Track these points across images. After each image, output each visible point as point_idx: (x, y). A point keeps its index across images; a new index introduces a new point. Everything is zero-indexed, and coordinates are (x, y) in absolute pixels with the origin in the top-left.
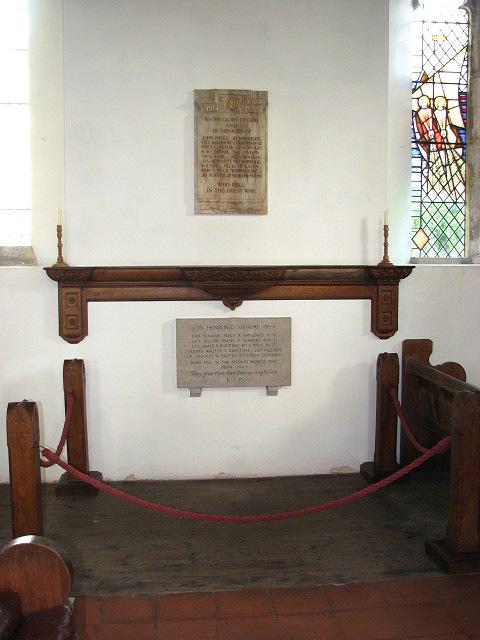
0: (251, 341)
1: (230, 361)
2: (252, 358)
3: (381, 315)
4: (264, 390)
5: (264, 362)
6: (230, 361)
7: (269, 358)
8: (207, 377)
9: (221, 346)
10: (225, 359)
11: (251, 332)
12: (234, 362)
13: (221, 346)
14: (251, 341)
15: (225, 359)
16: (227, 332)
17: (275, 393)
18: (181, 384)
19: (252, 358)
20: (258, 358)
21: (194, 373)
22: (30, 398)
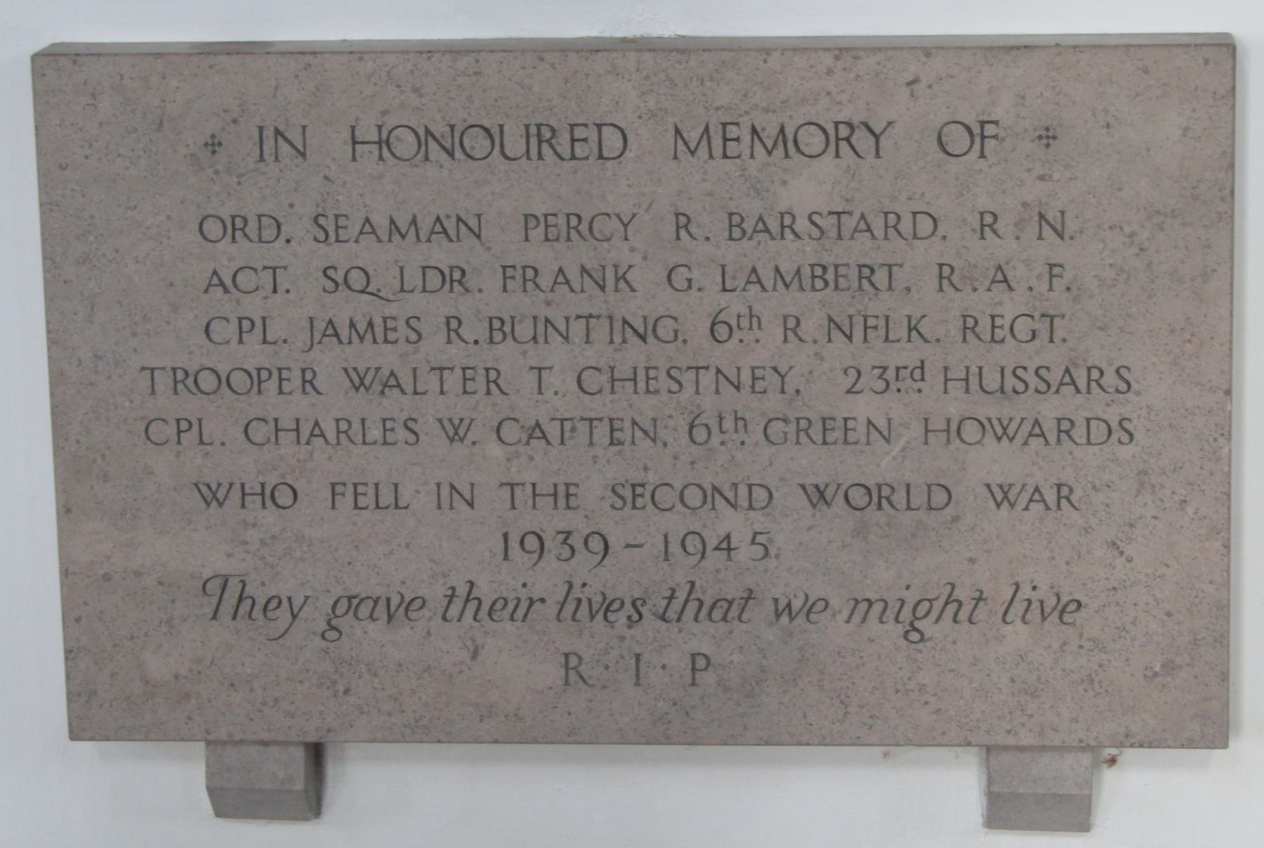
0: (822, 275)
1: (593, 487)
2: (813, 464)
3: (648, 58)
4: (958, 783)
5: (941, 495)
6: (593, 487)
7: (992, 462)
8: (369, 636)
9: (499, 328)
10: (539, 466)
11: (810, 187)
12: (631, 495)
13: (499, 328)
14: (822, 275)
15: (539, 466)
16: (549, 187)
17: (1074, 813)
18: (107, 701)
19: (813, 464)
20: (882, 464)
21: (231, 599)
22: (1095, 831)
